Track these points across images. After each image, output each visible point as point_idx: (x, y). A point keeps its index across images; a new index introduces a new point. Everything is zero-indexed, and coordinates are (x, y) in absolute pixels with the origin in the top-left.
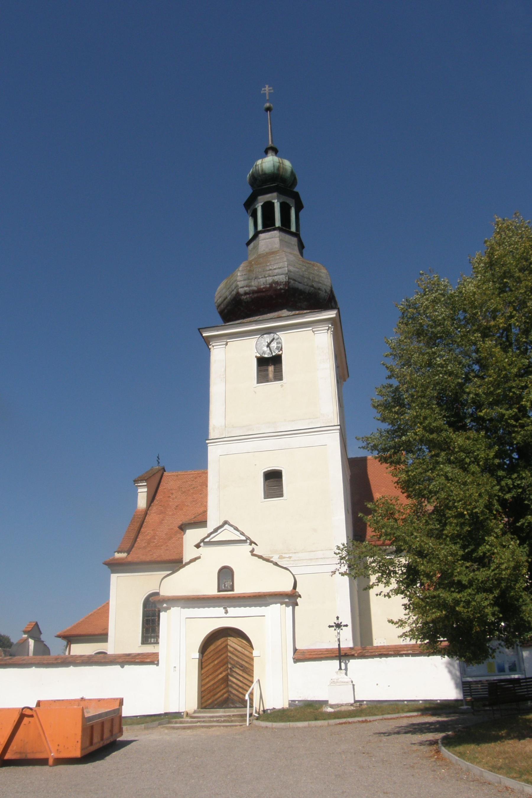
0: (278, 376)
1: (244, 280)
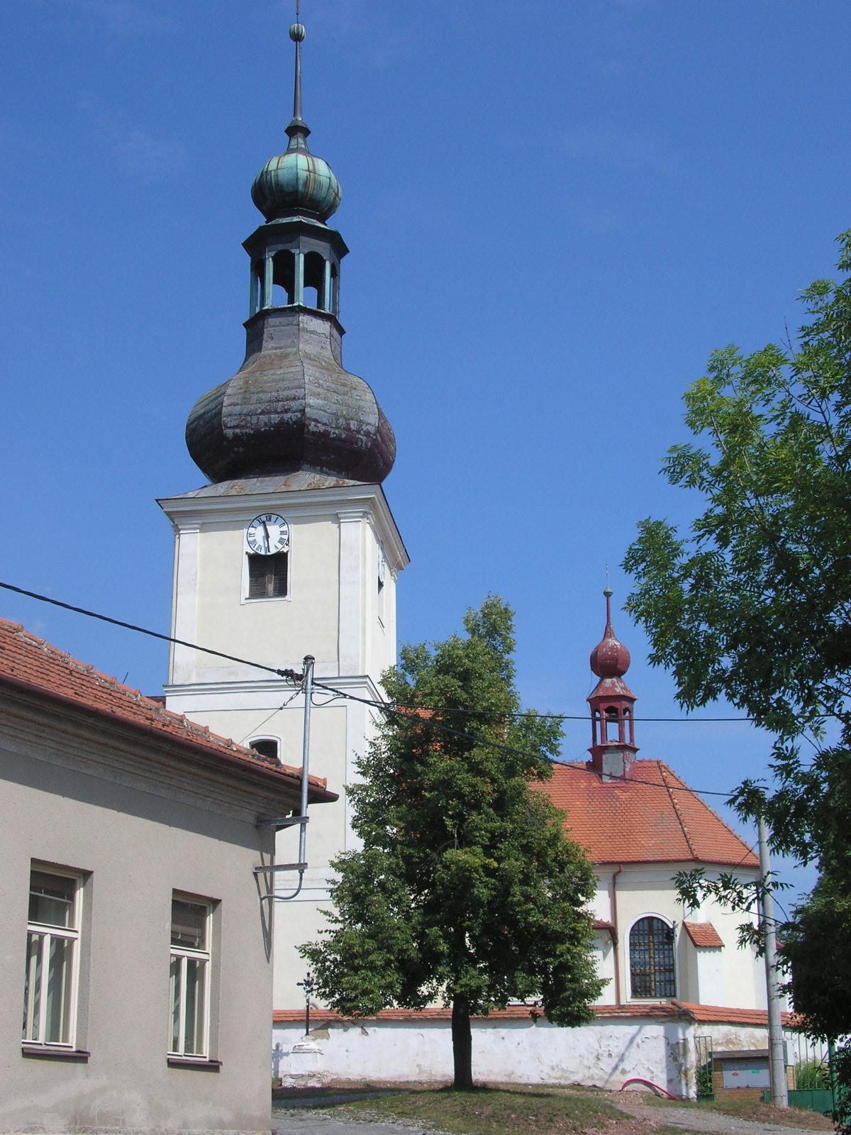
0: (282, 590)
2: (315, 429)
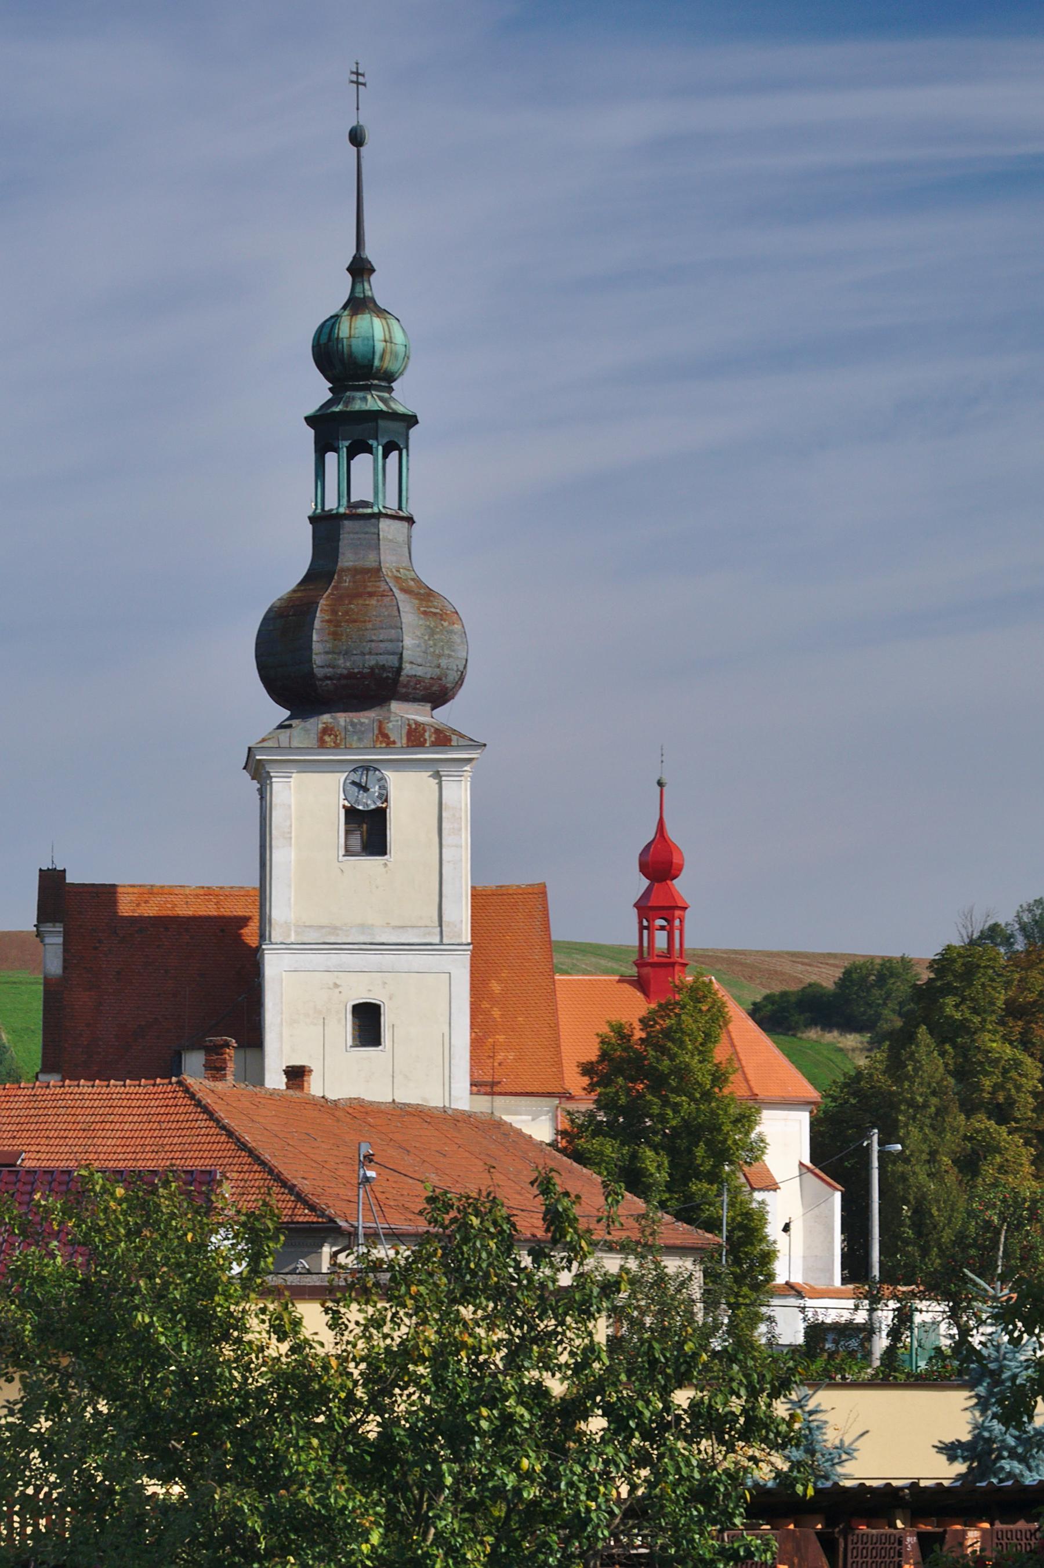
1: (327, 653)
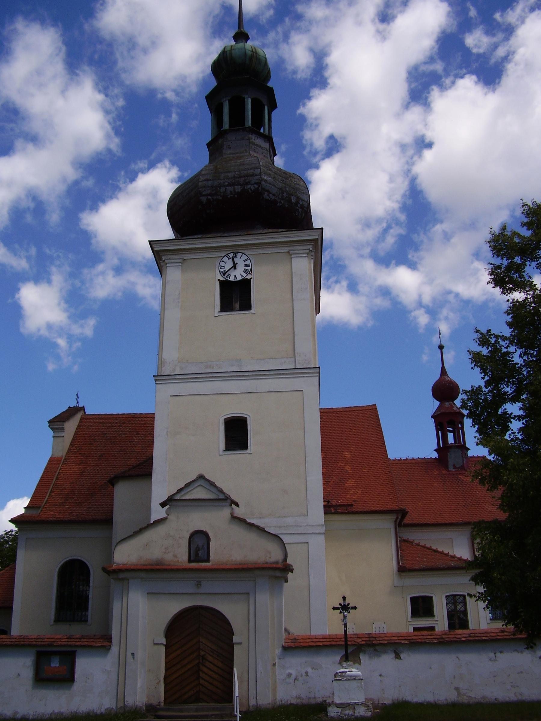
0: (246, 305)
2: (268, 198)
